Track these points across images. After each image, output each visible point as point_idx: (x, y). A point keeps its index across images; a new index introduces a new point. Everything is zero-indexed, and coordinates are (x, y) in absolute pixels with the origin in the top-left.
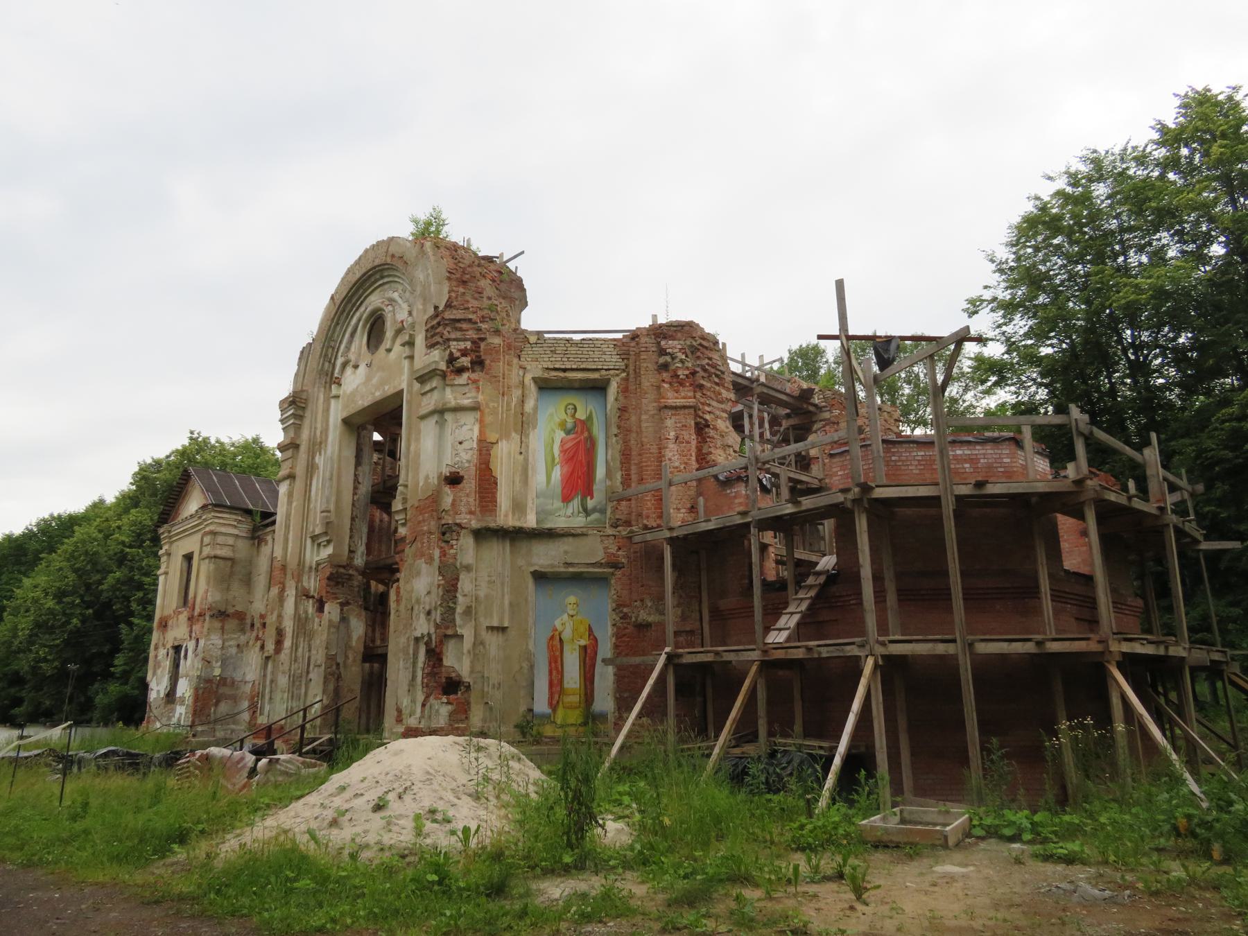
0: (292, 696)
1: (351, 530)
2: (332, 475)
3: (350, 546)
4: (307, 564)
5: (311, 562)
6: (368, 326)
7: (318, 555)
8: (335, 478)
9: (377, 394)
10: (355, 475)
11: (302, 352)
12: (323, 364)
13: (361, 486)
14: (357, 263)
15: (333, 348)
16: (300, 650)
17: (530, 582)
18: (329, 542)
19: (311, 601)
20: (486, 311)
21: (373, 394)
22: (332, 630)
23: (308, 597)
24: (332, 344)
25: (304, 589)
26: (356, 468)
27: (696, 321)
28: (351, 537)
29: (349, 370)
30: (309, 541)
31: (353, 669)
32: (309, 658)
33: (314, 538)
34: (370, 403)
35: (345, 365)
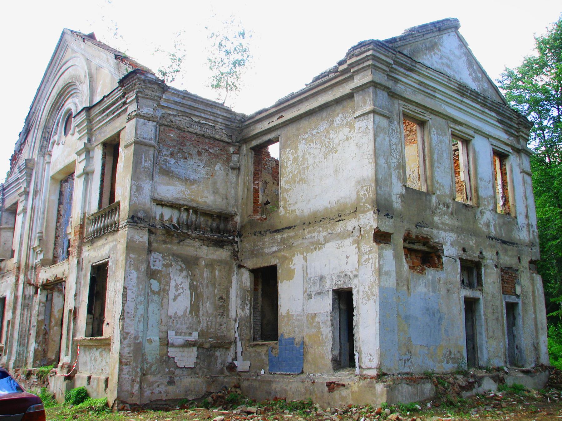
0: (20, 344)
1: (55, 244)
2: (44, 211)
3: (54, 254)
4: (30, 265)
5: (32, 264)
6: (65, 120)
7: (36, 259)
8: (46, 213)
9: (66, 161)
10: (58, 211)
11: (361, 45)
12: (43, 143)
13: (61, 217)
14: (462, 37)
15: (49, 133)
16: (25, 316)
17: (89, 375)
18: (41, 251)
19: (32, 287)
20: (415, 32)
21: (64, 161)
22: (42, 304)
23: (30, 284)
24: (48, 130)
25: (29, 280)
26: (59, 207)
27: (362, 40)
28: (55, 248)
29: (55, 146)
30: (32, 250)
31: (55, 328)
32: (30, 321)
33: (34, 249)
34: (63, 167)
35: (53, 144)
